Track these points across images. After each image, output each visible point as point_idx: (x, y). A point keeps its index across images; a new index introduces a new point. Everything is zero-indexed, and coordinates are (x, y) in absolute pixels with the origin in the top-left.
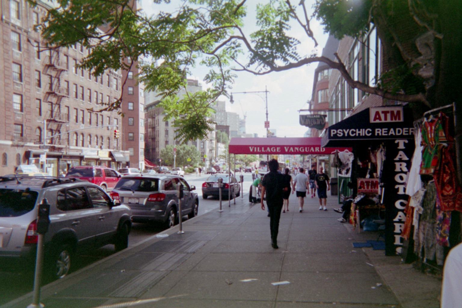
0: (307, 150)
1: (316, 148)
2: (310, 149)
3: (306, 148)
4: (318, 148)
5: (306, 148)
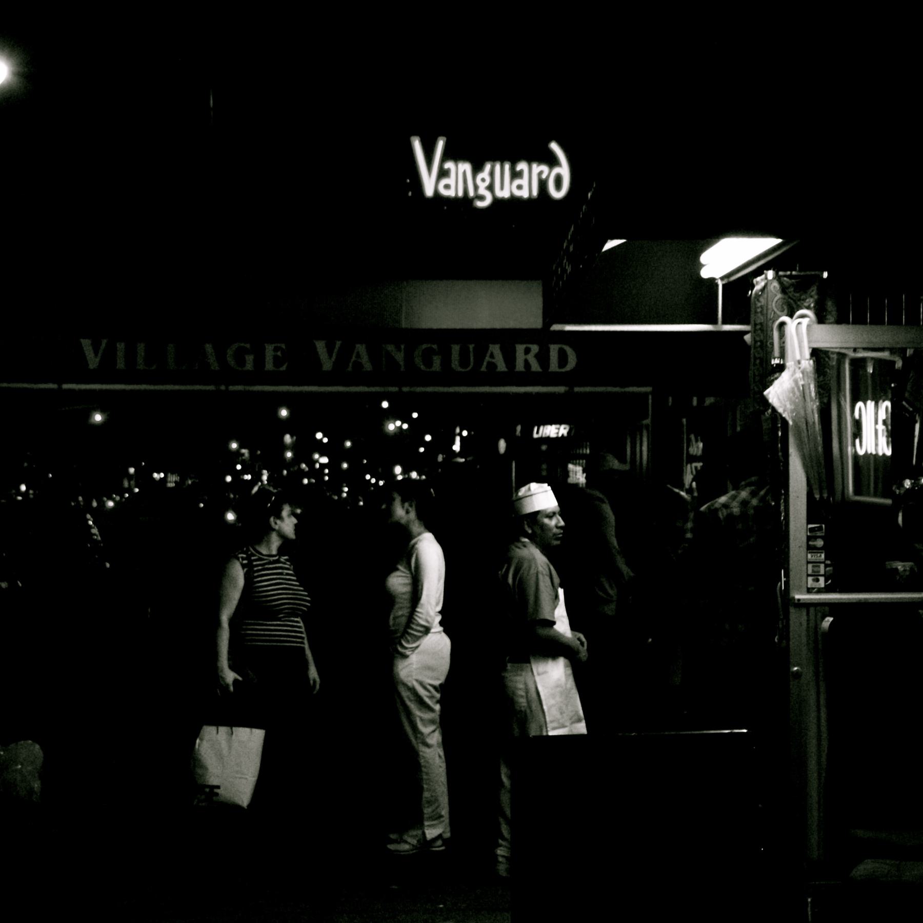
0: (464, 362)
1: (520, 348)
3: (456, 349)
4: (535, 348)
5: (456, 349)
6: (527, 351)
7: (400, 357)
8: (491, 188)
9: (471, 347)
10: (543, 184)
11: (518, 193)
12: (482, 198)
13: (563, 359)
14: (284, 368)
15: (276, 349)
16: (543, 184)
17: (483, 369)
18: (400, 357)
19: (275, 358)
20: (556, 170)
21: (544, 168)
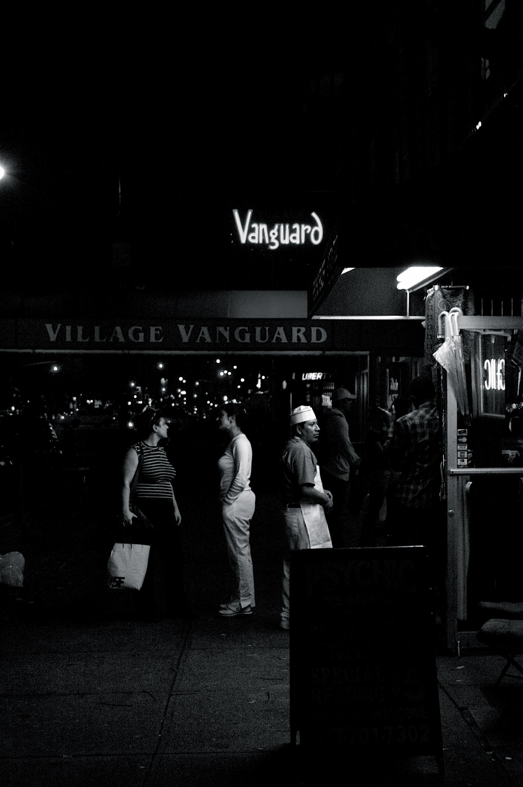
0: (263, 337)
1: (295, 329)
2: (272, 333)
3: (258, 329)
4: (303, 329)
5: (258, 329)
6: (299, 331)
7: (227, 334)
8: (278, 238)
9: (267, 328)
10: (308, 236)
11: (293, 241)
12: (273, 244)
13: (319, 335)
14: (161, 341)
15: (156, 330)
16: (308, 236)
17: (274, 341)
18: (227, 334)
19: (156, 335)
20: (315, 228)
21: (309, 227)
